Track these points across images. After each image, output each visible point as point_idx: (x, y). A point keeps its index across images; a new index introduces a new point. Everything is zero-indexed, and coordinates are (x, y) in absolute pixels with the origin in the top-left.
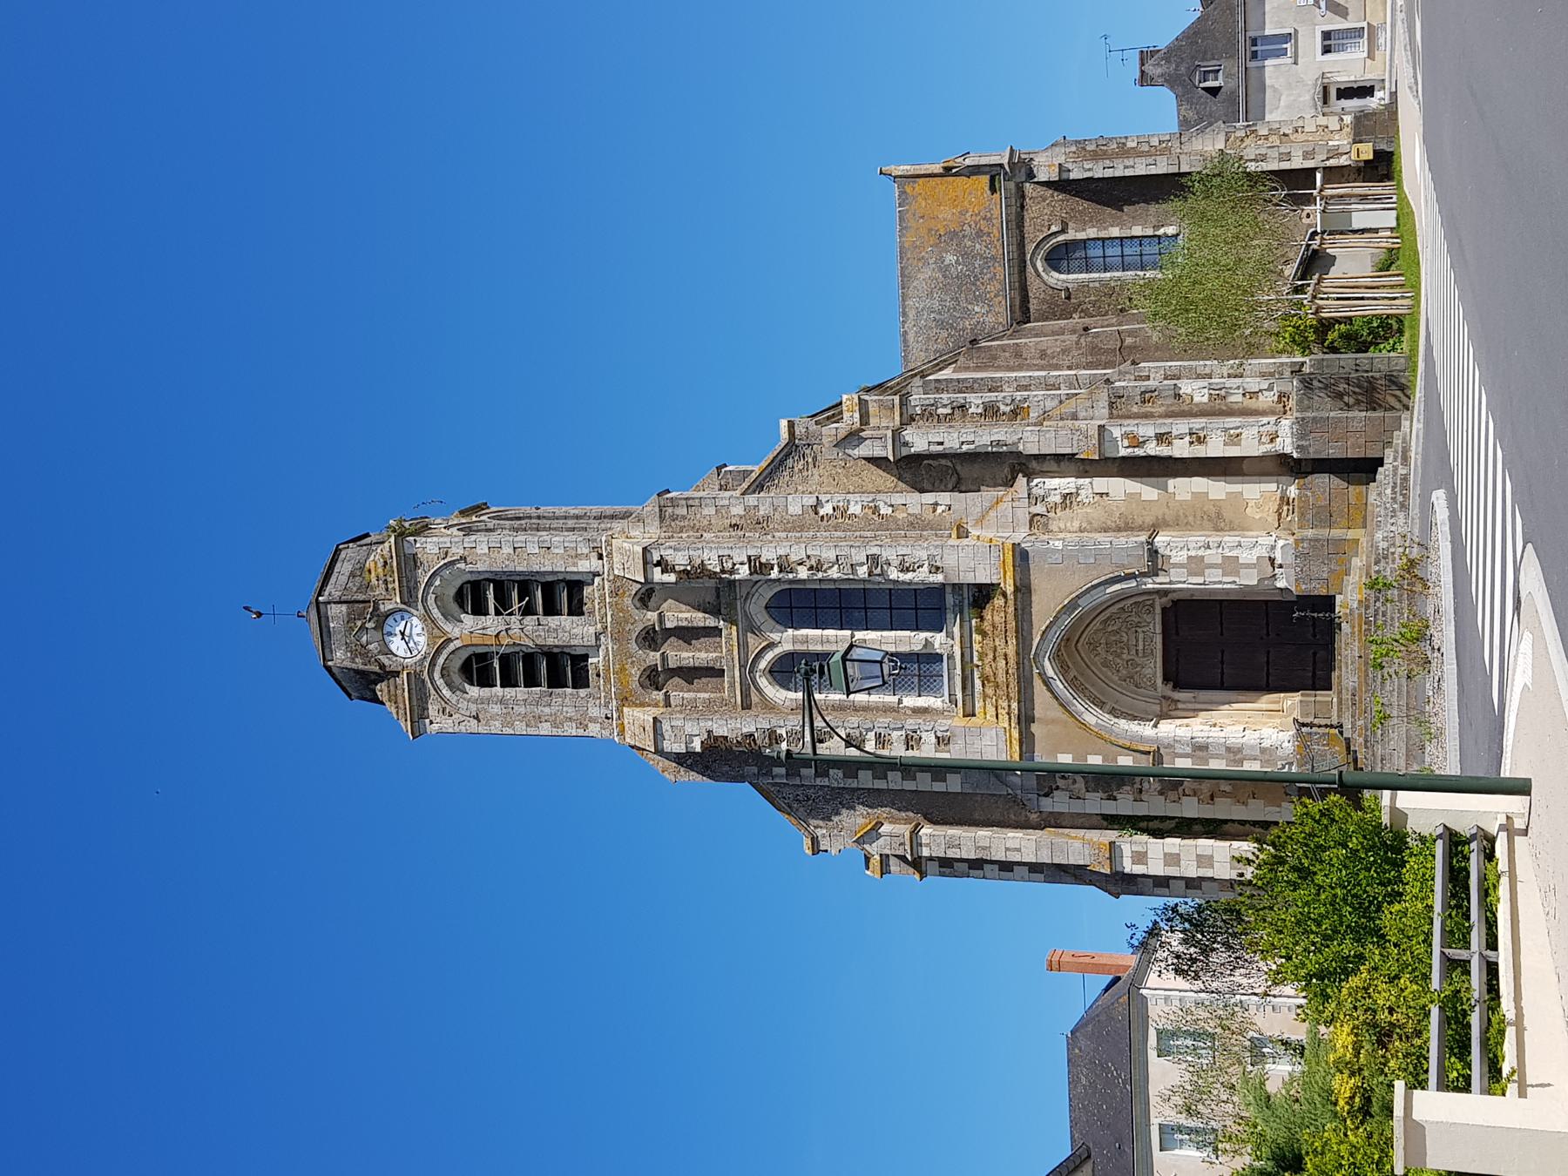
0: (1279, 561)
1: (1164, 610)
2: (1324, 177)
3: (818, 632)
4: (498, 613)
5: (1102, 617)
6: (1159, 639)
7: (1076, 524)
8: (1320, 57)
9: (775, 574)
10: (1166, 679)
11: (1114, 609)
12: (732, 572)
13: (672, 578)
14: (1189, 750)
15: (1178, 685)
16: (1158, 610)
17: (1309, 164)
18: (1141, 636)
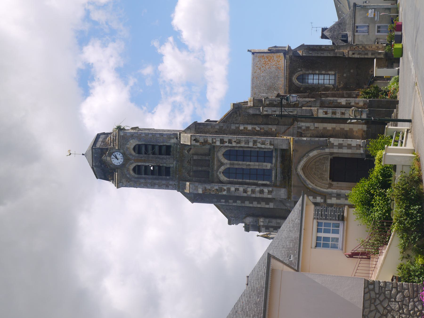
0: (361, 146)
1: (331, 159)
2: (376, 61)
3: (237, 162)
4: (145, 154)
5: (315, 161)
6: (329, 167)
7: (309, 135)
8: (376, 34)
9: (227, 144)
10: (330, 179)
11: (318, 159)
12: (215, 143)
13: (198, 144)
14: (335, 195)
15: (333, 181)
16: (329, 159)
17: (373, 57)
18: (324, 166)
